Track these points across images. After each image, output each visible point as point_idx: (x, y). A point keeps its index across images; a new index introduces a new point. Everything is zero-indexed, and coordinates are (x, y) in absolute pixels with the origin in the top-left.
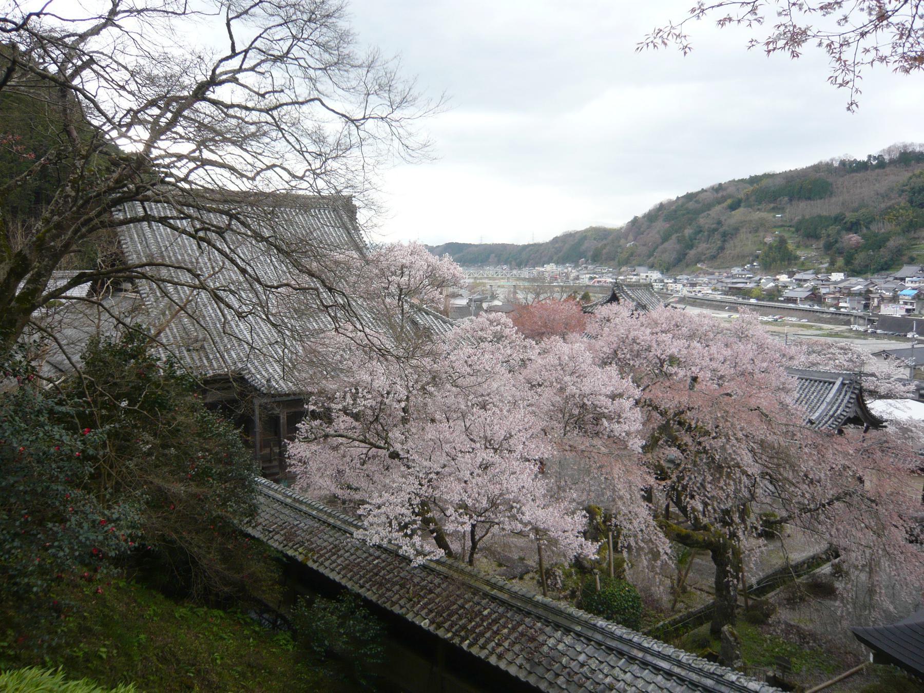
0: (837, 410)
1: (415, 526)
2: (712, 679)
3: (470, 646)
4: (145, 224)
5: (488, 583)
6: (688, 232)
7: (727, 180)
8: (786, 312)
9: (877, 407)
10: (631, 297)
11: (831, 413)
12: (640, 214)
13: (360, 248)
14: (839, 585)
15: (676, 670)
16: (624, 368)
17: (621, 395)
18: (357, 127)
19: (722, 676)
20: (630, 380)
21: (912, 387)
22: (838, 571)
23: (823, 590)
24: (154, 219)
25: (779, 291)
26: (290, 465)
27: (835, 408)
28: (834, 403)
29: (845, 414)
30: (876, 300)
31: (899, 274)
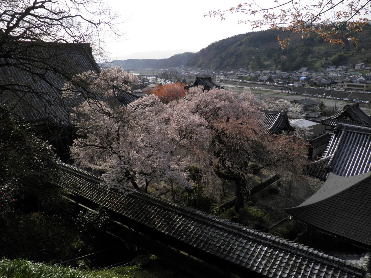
0: (279, 125)
1: (124, 181)
2: (237, 230)
3: (149, 223)
4: (6, 67)
5: (154, 200)
6: (224, 54)
7: (238, 34)
8: (259, 86)
9: (292, 122)
10: (203, 83)
11: (277, 126)
12: (205, 47)
13: (95, 67)
14: (280, 189)
15: (224, 228)
16: (202, 114)
17: (201, 125)
18: (96, 26)
19: (240, 229)
20: (204, 119)
21: (304, 115)
22: (279, 185)
23: (274, 192)
24: (11, 65)
25: (257, 77)
26: (72, 156)
27: (278, 124)
28: (278, 123)
29: (281, 127)
30: (292, 81)
31: (300, 71)
